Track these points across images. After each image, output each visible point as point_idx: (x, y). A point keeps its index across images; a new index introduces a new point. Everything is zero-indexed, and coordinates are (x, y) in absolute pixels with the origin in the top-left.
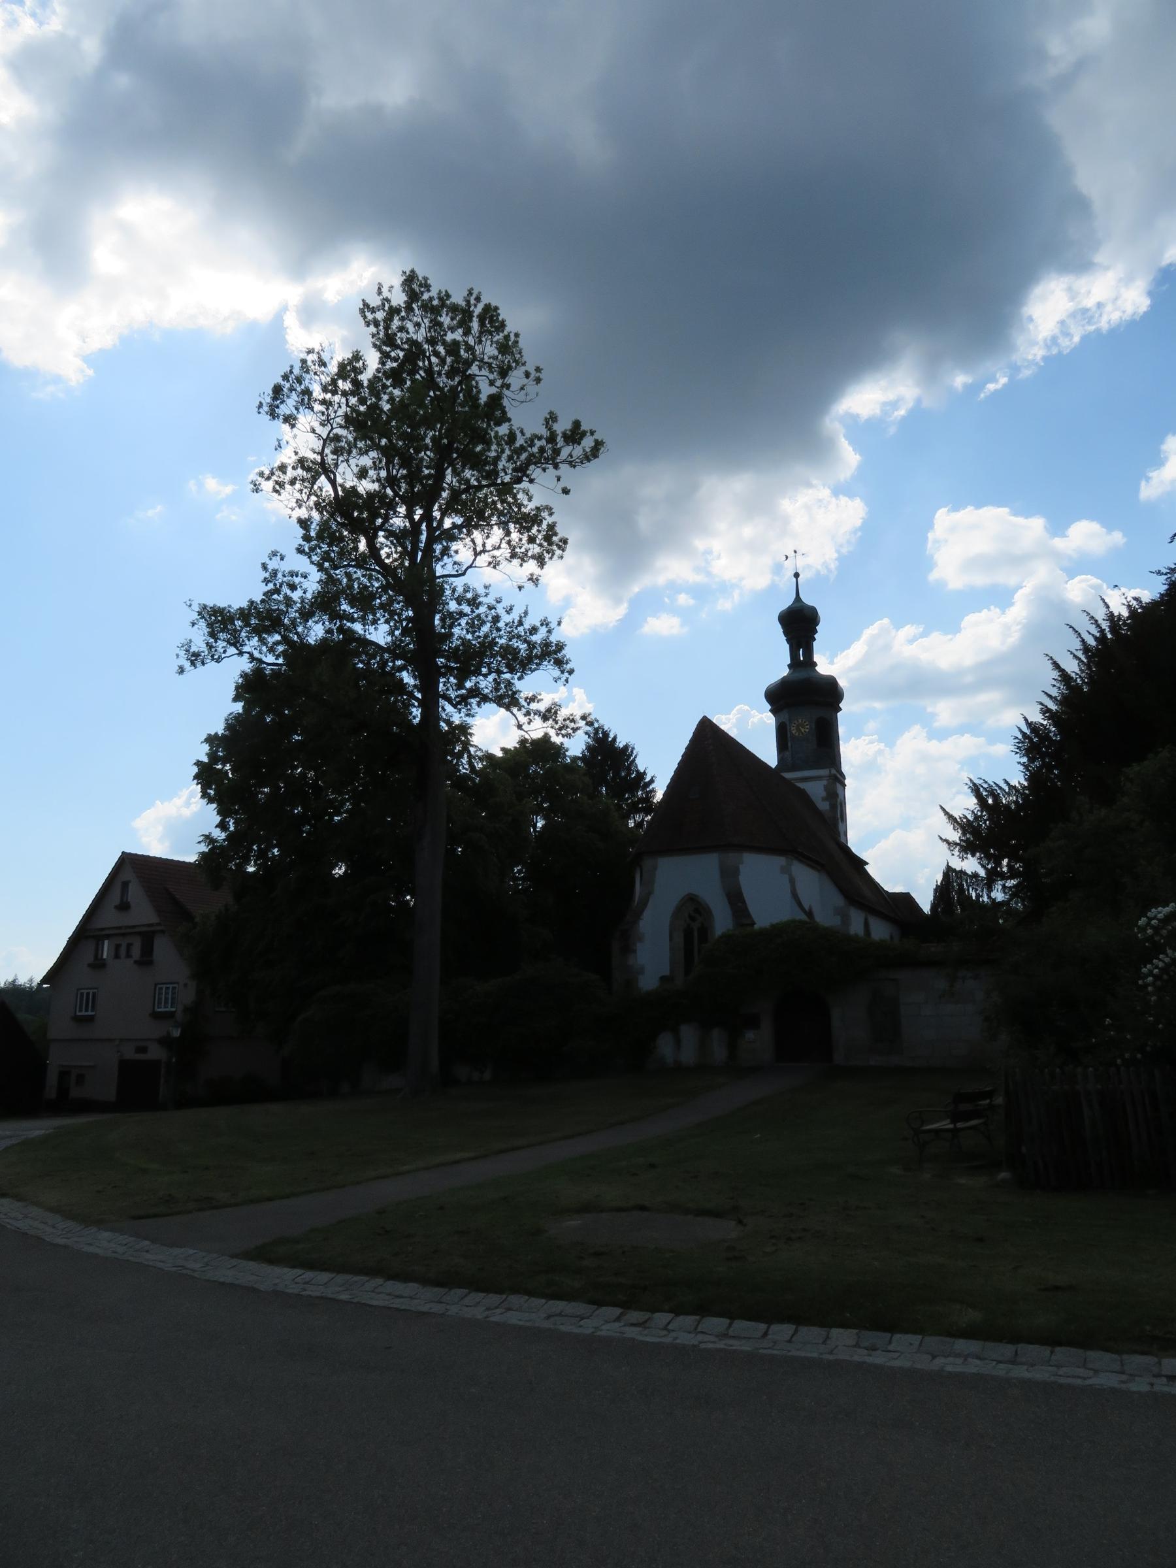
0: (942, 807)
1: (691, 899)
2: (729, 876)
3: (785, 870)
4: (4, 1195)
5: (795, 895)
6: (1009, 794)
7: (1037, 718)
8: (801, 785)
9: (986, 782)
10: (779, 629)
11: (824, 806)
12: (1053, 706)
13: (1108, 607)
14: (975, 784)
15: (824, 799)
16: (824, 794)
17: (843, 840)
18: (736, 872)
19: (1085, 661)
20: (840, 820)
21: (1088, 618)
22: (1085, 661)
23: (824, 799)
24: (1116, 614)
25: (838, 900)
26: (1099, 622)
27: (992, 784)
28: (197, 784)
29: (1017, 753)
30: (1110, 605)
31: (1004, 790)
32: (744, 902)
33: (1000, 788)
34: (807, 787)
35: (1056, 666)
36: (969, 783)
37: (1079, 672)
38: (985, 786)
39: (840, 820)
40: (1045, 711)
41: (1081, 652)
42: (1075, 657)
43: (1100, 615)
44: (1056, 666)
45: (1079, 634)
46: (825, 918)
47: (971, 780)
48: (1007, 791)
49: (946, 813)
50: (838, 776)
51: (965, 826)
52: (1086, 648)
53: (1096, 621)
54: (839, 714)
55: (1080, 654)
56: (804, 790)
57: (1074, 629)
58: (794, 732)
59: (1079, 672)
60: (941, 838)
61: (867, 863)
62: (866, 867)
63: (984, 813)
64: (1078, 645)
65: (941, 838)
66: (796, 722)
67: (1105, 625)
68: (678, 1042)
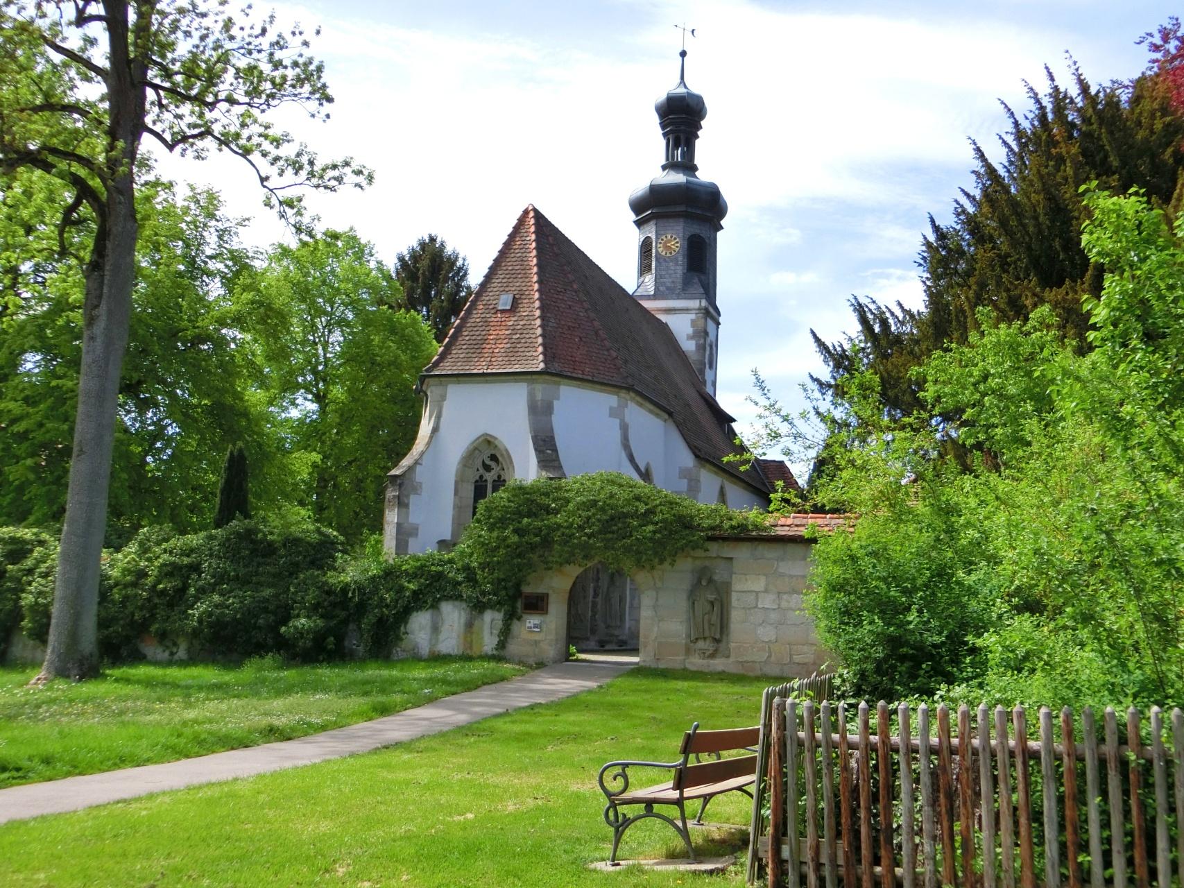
0: (812, 332)
1: (488, 441)
2: (540, 414)
3: (613, 413)
4: (4, 769)
5: (626, 445)
6: (902, 323)
7: (948, 221)
8: (663, 318)
9: (874, 302)
10: (655, 119)
11: (689, 346)
12: (971, 209)
13: (1052, 79)
14: (860, 305)
15: (690, 338)
16: (690, 331)
17: (709, 389)
18: (548, 409)
19: (1016, 149)
20: (707, 366)
21: (1026, 89)
22: (1016, 149)
23: (690, 338)
24: (1062, 89)
25: (686, 458)
26: (1039, 96)
27: (885, 310)
28: (248, 401)
29: (920, 265)
30: (1056, 77)
31: (897, 317)
32: (555, 450)
33: (892, 314)
34: (672, 321)
35: (981, 155)
36: (853, 301)
37: (1007, 164)
38: (872, 307)
39: (707, 366)
40: (960, 211)
41: (1013, 137)
42: (1005, 143)
43: (1044, 89)
44: (981, 155)
45: (1012, 113)
46: (667, 485)
47: (855, 298)
48: (901, 318)
49: (817, 340)
50: (711, 310)
51: (841, 360)
52: (1019, 133)
53: (1036, 94)
54: (720, 234)
55: (1010, 139)
56: (666, 324)
57: (1006, 106)
58: (660, 250)
59: (1007, 164)
60: (811, 377)
61: (734, 420)
62: (733, 425)
63: (869, 345)
64: (1010, 127)
65: (811, 377)
66: (664, 237)
67: (1048, 103)
68: (436, 629)
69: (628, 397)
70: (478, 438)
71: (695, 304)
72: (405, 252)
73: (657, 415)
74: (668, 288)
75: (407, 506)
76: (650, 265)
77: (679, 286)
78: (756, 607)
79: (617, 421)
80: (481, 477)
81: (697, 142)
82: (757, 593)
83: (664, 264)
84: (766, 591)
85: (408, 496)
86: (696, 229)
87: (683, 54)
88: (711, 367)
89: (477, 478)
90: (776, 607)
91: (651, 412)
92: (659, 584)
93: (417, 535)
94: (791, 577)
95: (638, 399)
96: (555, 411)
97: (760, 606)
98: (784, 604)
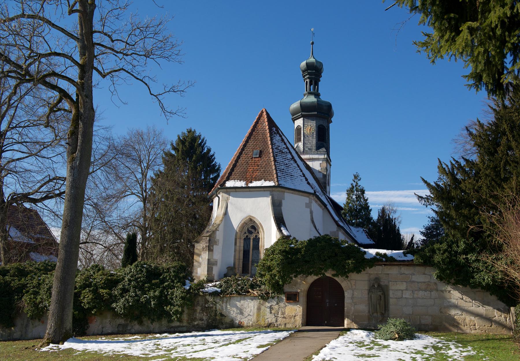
3: (308, 205)
69: (313, 198)
70: (247, 217)
71: (322, 157)
72: (180, 134)
73: (321, 207)
74: (309, 149)
75: (212, 250)
76: (300, 139)
77: (314, 148)
78: (402, 297)
79: (309, 209)
80: (247, 236)
81: (320, 83)
82: (402, 291)
83: (307, 138)
84: (407, 290)
85: (213, 246)
86: (321, 122)
87: (313, 43)
88: (328, 185)
89: (245, 237)
90: (412, 297)
91: (319, 205)
92: (354, 287)
93: (217, 264)
94: (418, 283)
95: (316, 199)
96: (283, 205)
97: (404, 296)
98: (415, 296)
